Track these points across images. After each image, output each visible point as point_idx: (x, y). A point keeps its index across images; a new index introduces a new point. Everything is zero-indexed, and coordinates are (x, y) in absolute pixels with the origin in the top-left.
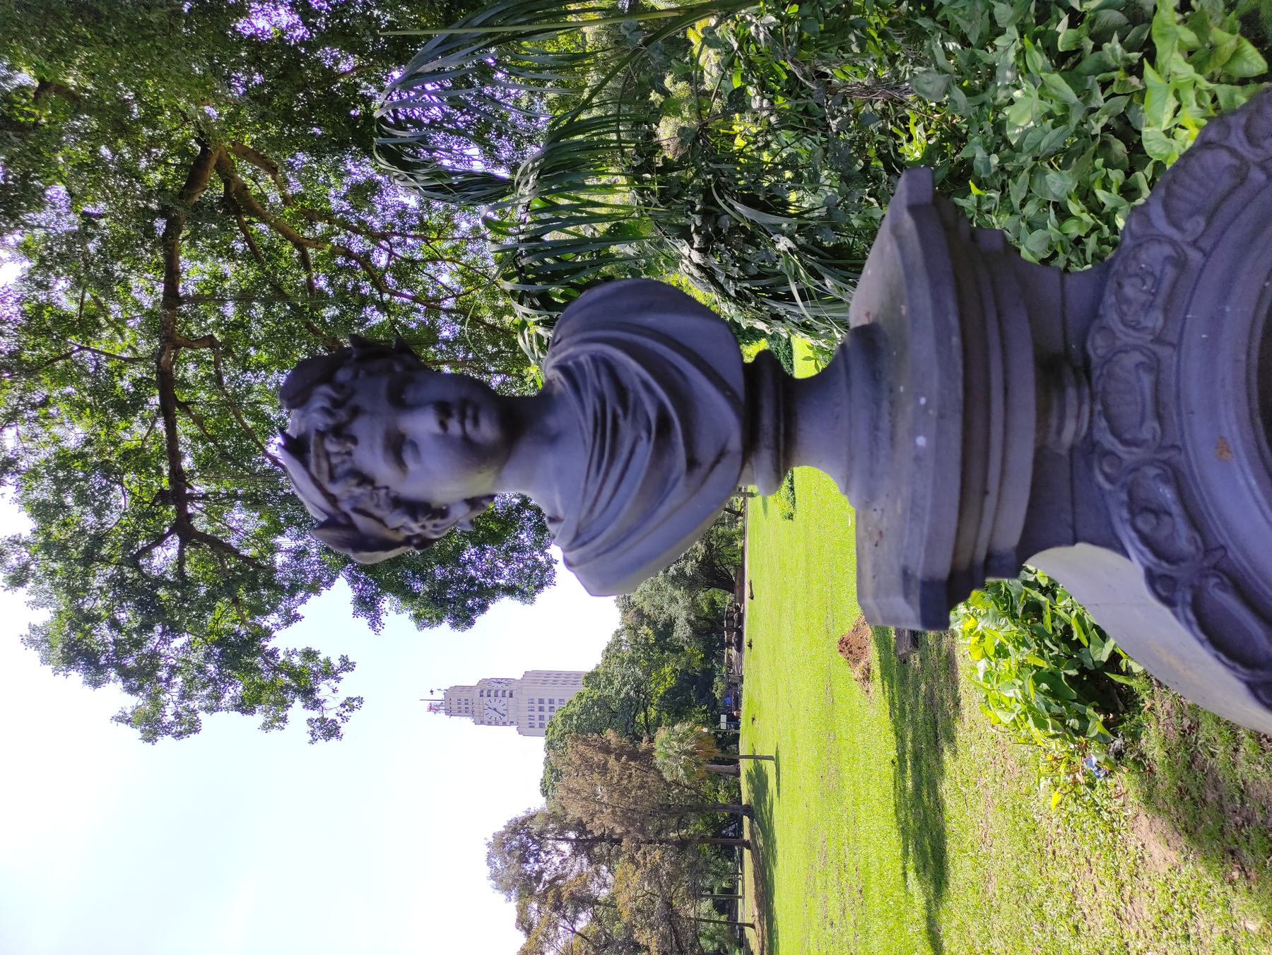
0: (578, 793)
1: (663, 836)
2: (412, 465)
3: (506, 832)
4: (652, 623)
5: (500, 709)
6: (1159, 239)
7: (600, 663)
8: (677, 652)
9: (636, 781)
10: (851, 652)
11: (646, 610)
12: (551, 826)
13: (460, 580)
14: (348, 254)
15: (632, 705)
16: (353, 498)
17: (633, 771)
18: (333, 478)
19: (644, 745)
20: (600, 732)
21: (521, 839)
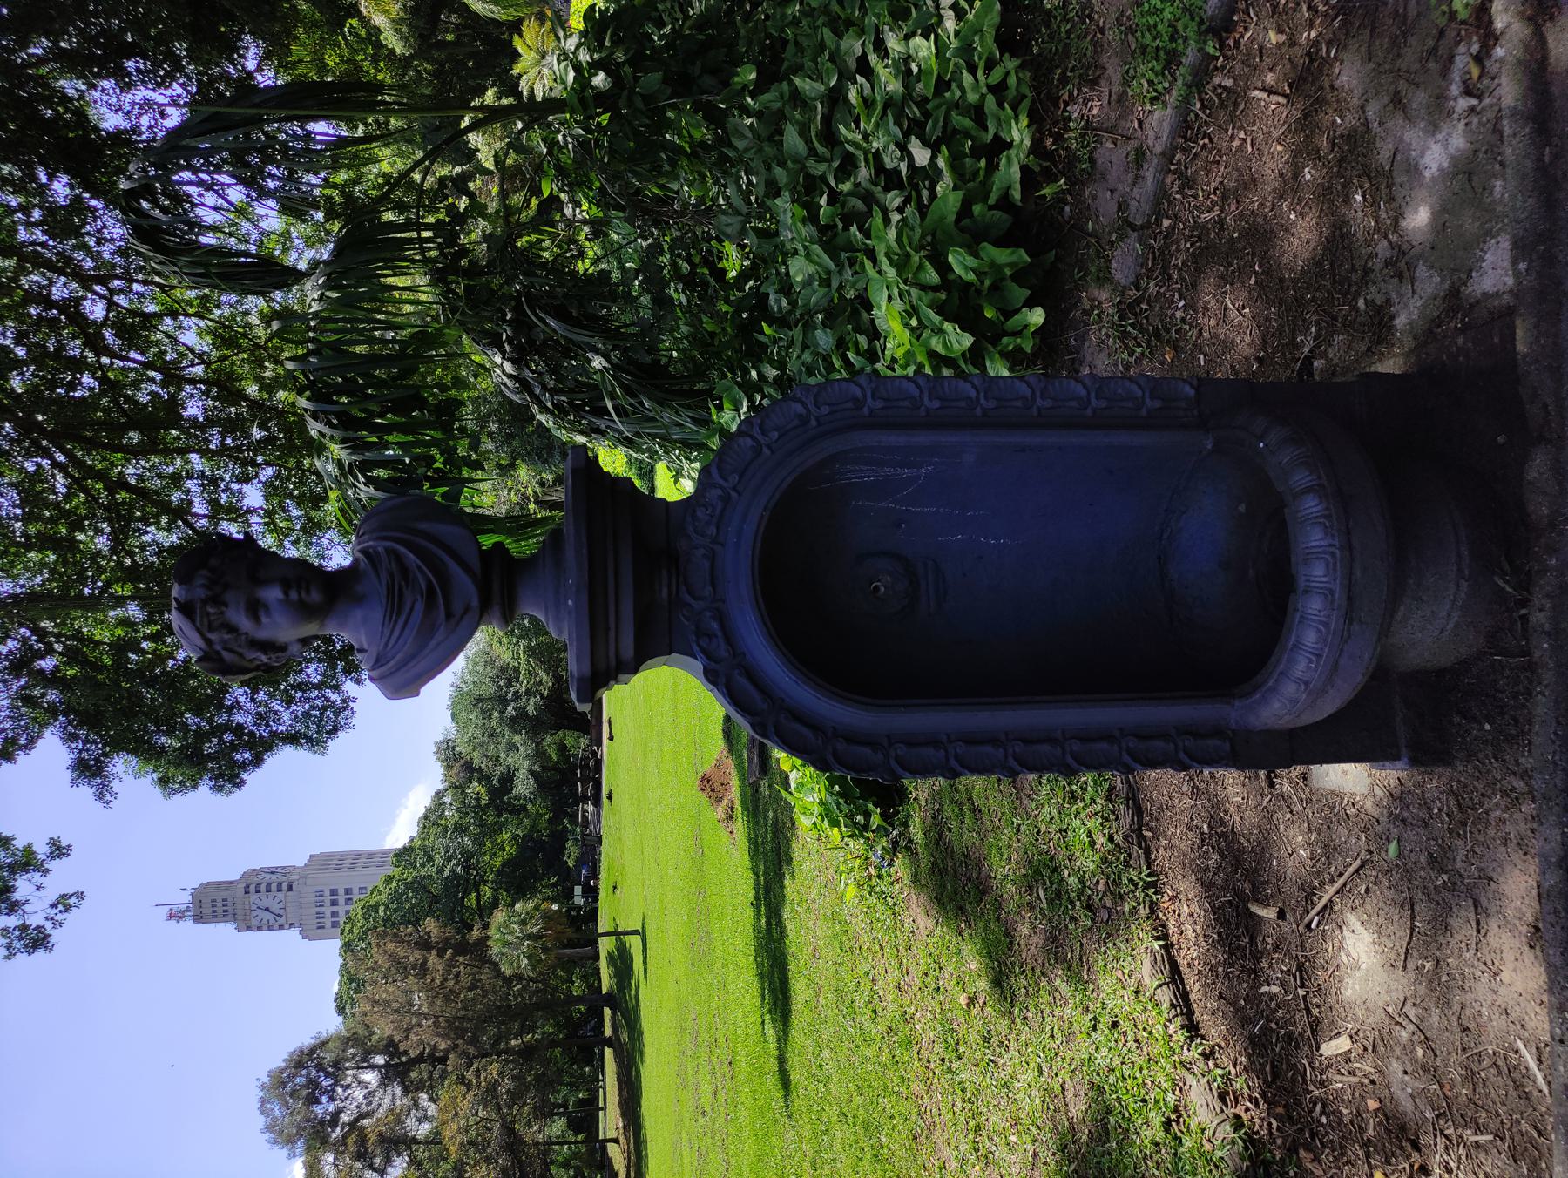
0: (387, 1003)
2: (264, 620)
4: (484, 778)
5: (275, 908)
7: (415, 834)
9: (465, 981)
10: (713, 790)
11: (476, 761)
14: (48, 303)
15: (459, 884)
17: (462, 968)
18: (211, 630)
20: (416, 924)
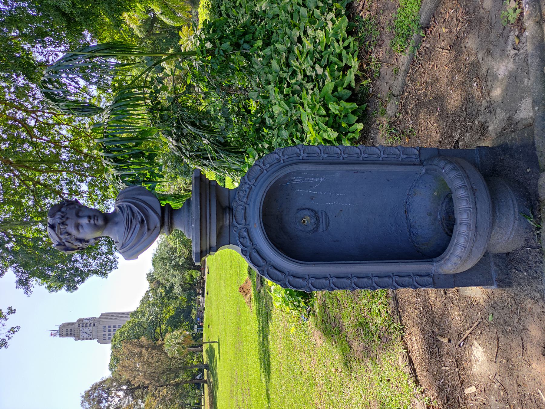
1: (168, 383)
2: (81, 231)
3: (91, 390)
4: (164, 287)
5: (89, 332)
6: (246, 183)
7: (139, 306)
8: (175, 299)
9: (155, 359)
11: (161, 281)
12: (114, 384)
13: (72, 269)
14: (15, 120)
15: (154, 325)
16: (66, 239)
17: (154, 354)
18: (61, 234)
19: (159, 342)
20: (138, 339)
21: (99, 392)
